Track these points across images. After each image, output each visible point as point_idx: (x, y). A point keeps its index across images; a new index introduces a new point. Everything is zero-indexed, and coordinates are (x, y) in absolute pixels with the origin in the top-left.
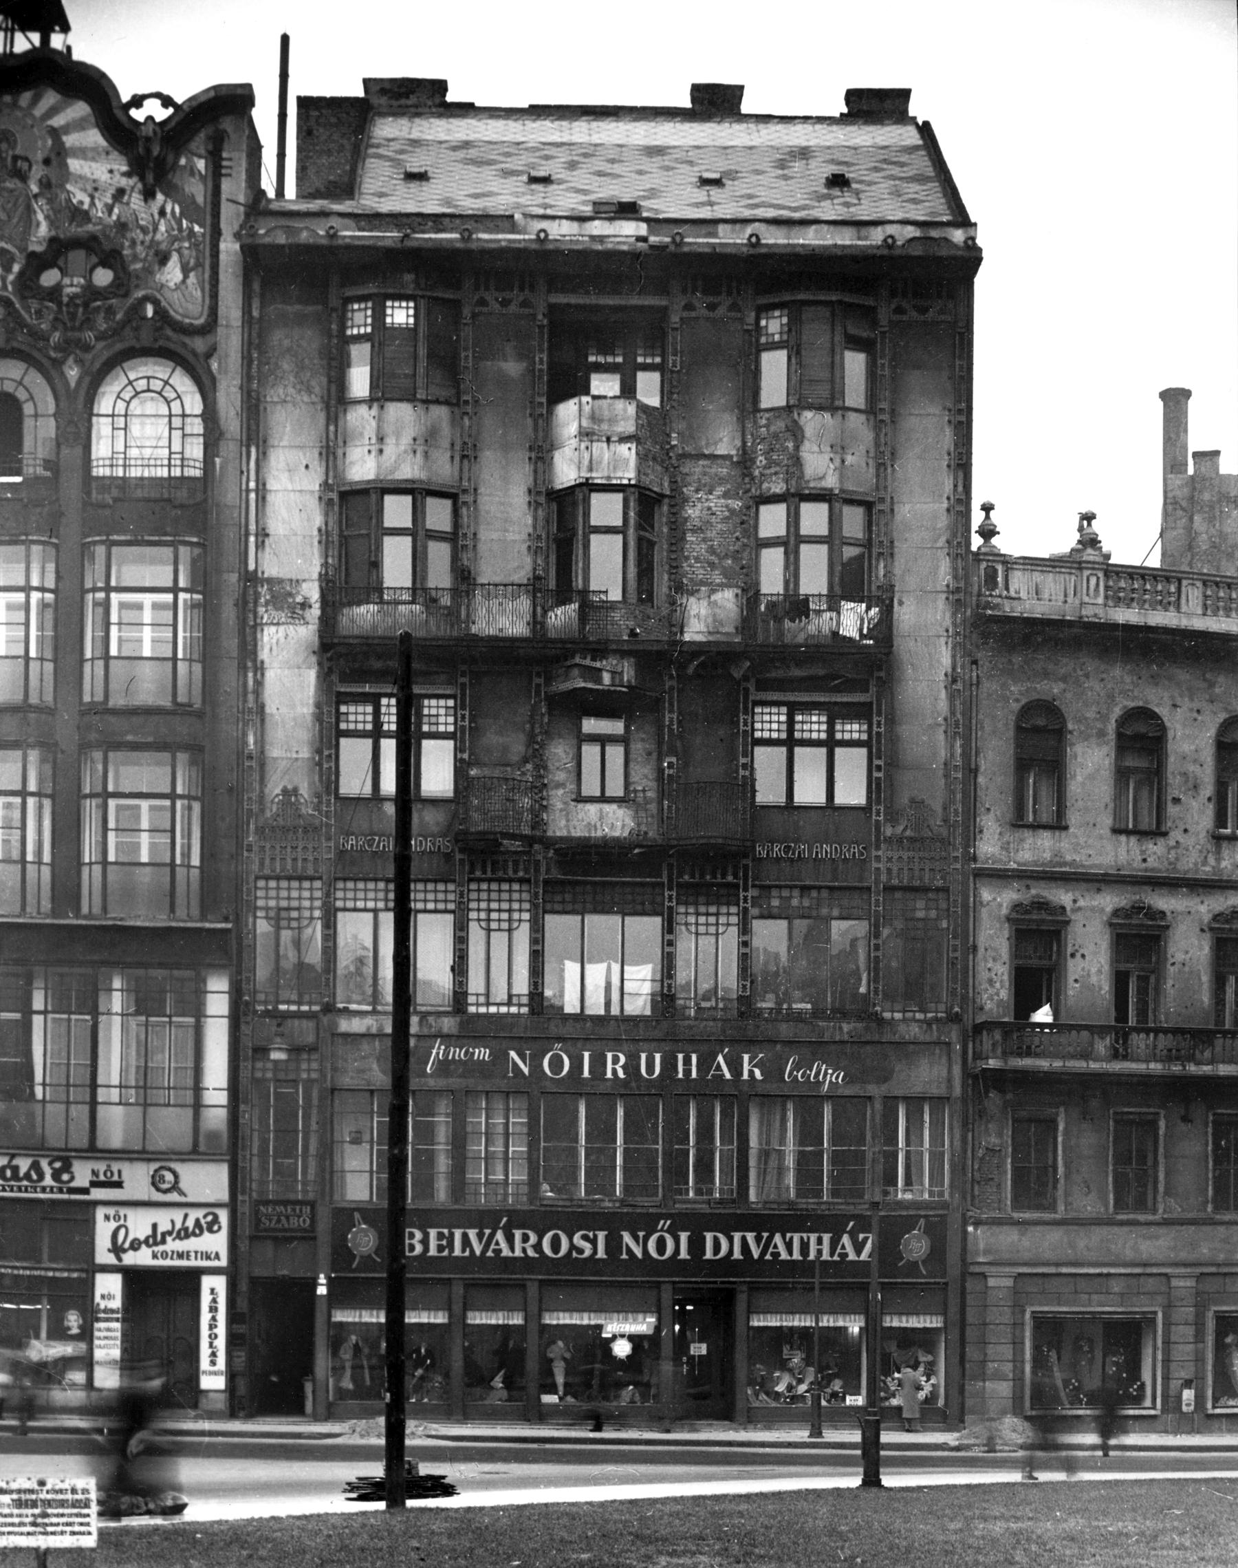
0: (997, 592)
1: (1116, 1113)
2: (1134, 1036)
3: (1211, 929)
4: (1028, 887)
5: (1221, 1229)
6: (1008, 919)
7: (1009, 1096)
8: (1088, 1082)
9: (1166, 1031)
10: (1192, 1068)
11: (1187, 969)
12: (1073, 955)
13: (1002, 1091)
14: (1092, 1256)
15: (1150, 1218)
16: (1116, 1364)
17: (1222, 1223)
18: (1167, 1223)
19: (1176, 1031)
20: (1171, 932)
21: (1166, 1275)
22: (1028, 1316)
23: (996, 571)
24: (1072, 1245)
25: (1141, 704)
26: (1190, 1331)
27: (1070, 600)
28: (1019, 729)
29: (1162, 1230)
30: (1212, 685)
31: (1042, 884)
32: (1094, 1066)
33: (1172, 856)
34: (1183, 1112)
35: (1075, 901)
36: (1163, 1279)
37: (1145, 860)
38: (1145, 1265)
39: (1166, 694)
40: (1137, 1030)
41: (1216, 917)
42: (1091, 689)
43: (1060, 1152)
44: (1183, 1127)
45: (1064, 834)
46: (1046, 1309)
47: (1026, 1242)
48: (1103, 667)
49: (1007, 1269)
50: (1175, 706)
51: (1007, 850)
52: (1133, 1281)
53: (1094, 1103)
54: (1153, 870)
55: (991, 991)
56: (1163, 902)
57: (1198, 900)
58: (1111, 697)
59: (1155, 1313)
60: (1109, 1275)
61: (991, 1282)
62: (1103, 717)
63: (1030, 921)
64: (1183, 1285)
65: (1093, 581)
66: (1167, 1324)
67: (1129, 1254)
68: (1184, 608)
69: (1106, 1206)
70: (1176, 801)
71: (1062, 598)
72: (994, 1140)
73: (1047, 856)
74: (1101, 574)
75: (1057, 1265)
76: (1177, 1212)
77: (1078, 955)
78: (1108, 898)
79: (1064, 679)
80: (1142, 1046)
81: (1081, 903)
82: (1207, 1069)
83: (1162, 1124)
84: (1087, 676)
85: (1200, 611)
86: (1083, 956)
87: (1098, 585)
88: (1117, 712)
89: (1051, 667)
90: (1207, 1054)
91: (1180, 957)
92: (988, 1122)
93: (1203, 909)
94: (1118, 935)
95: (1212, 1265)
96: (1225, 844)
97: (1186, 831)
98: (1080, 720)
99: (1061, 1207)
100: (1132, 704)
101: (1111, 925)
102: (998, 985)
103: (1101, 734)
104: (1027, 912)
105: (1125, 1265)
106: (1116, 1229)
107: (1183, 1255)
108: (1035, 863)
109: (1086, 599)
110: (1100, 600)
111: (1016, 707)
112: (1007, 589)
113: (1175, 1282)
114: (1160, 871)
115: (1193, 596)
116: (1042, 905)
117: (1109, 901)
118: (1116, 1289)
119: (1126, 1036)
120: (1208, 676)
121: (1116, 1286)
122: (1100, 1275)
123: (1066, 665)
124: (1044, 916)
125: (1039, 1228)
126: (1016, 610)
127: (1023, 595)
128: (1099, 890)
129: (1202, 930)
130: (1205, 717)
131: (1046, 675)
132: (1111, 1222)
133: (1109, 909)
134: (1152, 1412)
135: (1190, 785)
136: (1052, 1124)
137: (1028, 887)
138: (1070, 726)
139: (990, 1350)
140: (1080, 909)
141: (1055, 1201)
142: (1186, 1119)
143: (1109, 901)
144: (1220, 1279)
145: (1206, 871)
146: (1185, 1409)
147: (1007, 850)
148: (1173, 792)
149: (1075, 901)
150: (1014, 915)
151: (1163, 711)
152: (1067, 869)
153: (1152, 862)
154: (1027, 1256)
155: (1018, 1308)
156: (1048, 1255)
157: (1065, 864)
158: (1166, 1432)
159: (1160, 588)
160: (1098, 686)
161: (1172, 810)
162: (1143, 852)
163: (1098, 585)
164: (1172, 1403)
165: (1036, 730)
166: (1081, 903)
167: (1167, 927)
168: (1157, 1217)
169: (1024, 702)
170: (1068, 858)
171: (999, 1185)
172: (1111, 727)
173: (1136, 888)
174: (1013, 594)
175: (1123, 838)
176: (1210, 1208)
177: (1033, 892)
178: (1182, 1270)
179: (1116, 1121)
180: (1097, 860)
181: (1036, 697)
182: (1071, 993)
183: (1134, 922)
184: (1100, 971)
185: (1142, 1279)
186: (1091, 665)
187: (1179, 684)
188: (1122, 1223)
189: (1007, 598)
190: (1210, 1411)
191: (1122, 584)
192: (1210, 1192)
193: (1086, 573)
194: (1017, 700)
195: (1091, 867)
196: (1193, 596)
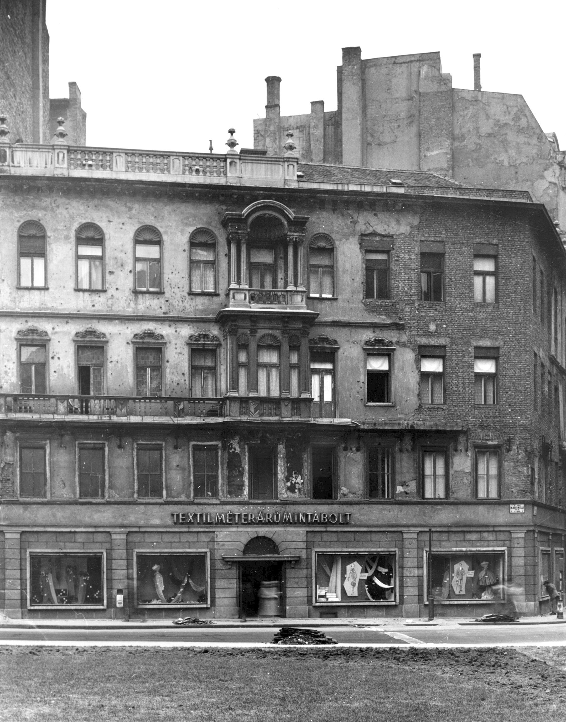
0: (6, 163)
1: (79, 444)
2: (92, 401)
3: (133, 343)
4: (26, 321)
5: (142, 507)
6: (16, 339)
7: (18, 435)
8: (62, 426)
9: (105, 398)
10: (115, 419)
11: (119, 365)
12: (53, 358)
13: (14, 432)
14: (64, 522)
15: (99, 500)
16: (85, 581)
17: (142, 504)
18: (108, 503)
19: (110, 398)
20: (109, 344)
21: (109, 532)
22: (28, 555)
23: (5, 152)
24: (54, 516)
25: (89, 221)
26: (124, 563)
27: (48, 166)
28: (20, 237)
29: (107, 507)
30: (130, 209)
31: (35, 319)
32: (58, 418)
33: (110, 302)
34: (118, 442)
35: (53, 329)
36: (108, 535)
37: (93, 306)
38: (95, 527)
39: (104, 216)
40: (95, 398)
41: (135, 336)
42: (61, 214)
43: (47, 465)
44: (119, 451)
45: (46, 292)
46: (38, 550)
47: (27, 514)
48: (67, 201)
49: (413, 529)
50: (109, 221)
51: (14, 301)
52: (90, 536)
53: (67, 438)
54: (98, 311)
55: (7, 378)
56: (102, 327)
57: (126, 326)
58: (72, 218)
59: (102, 553)
60: (75, 532)
61: (8, 536)
62: (68, 229)
63: (27, 339)
64: (119, 537)
65: (61, 155)
66: (510, 556)
67: (87, 520)
68: (114, 168)
69: (75, 494)
70: (111, 273)
71: (44, 165)
72: (9, 459)
73: (37, 305)
74: (65, 152)
75: (44, 526)
76: (117, 498)
77: (56, 358)
78: (73, 327)
79: (45, 209)
80: (97, 407)
81: (57, 329)
82: (124, 419)
83: (107, 449)
84: (58, 207)
85: (124, 170)
86: (59, 358)
87: (64, 157)
88: (76, 226)
89: (37, 202)
90: (124, 410)
91: (115, 358)
92: (5, 449)
93: (128, 332)
94: (137, 348)
95: (137, 527)
96: (140, 296)
97: (117, 289)
98: (56, 230)
99: (48, 495)
100: (84, 221)
101: (74, 341)
102: (10, 375)
103: (67, 238)
104: (83, 337)
105: (85, 526)
106: (79, 507)
107: (120, 521)
108: (31, 309)
109: (57, 165)
110: (65, 165)
111: (18, 225)
112: (13, 162)
113: (114, 536)
114: (102, 311)
115: (120, 162)
116: (92, 333)
117: (74, 328)
118: (80, 540)
119: (87, 401)
120: (128, 204)
121: (80, 538)
122: (70, 532)
123: (46, 201)
124: (36, 337)
125: (34, 506)
126: (14, 172)
127: (22, 165)
128: (67, 322)
129: (128, 343)
130: (126, 227)
131: (34, 207)
132: (75, 503)
133: (74, 333)
134: (394, 603)
135: (119, 264)
136: (43, 448)
137: (26, 321)
138: (49, 234)
139: (8, 572)
140: (56, 333)
141: (45, 492)
142: (120, 447)
143: (74, 328)
144: (142, 535)
145: (129, 311)
146: (118, 605)
147: (14, 301)
148: (109, 268)
149: (53, 329)
150: (19, 337)
151: (102, 225)
152: (49, 311)
153: (97, 307)
154: (28, 522)
155: (22, 549)
156: (40, 521)
157: (48, 309)
158: (111, 618)
159: (144, 160)
160: (64, 212)
161: (108, 277)
162: (92, 301)
163: (64, 157)
164: (111, 601)
165: (30, 237)
166: (57, 329)
167: (107, 342)
168: (103, 501)
169: (22, 221)
170: (49, 305)
171: (13, 483)
172: (73, 234)
173: (90, 321)
174: (16, 164)
175: (81, 294)
176: (136, 496)
177: (30, 324)
178: (118, 530)
179: (80, 449)
180: (65, 306)
181: (30, 219)
182: (52, 378)
183: (29, 337)
184: (69, 366)
185: (95, 534)
186: (61, 201)
187: (112, 210)
188: (83, 504)
189: (14, 166)
190: (29, 608)
191: (137, 160)
192: (136, 488)
193: (57, 151)
194: (18, 221)
195: (61, 310)
196: (120, 162)
